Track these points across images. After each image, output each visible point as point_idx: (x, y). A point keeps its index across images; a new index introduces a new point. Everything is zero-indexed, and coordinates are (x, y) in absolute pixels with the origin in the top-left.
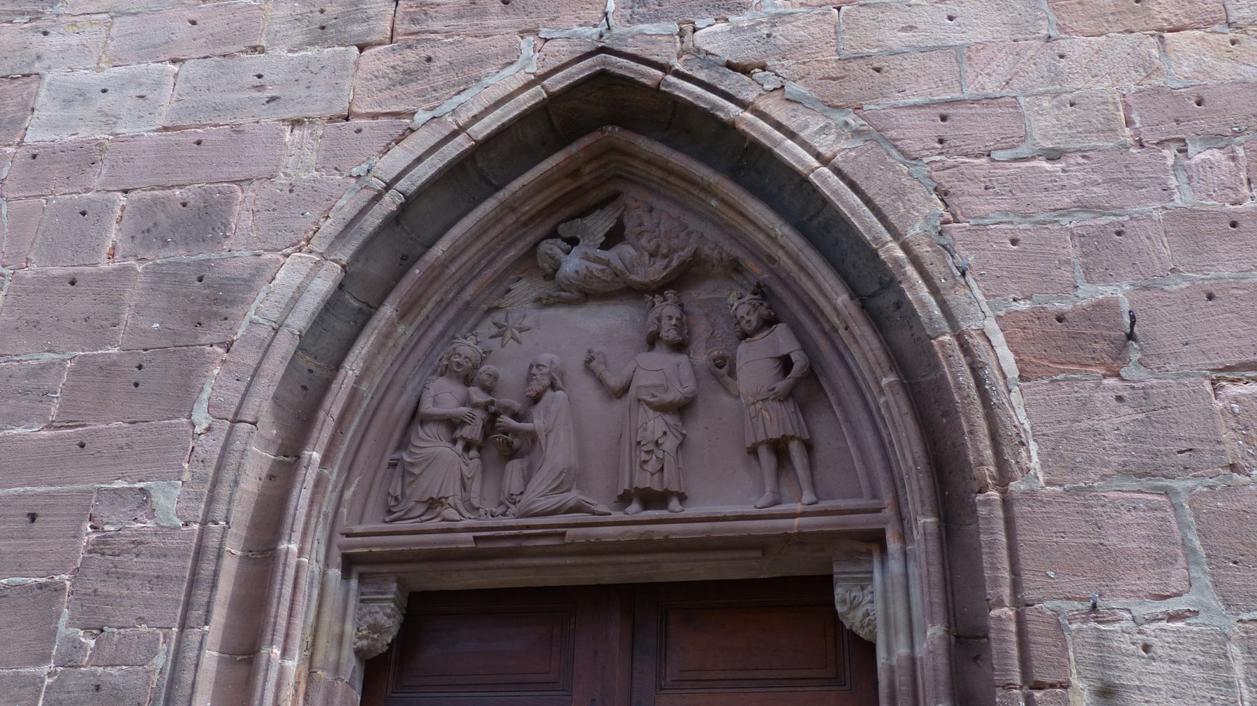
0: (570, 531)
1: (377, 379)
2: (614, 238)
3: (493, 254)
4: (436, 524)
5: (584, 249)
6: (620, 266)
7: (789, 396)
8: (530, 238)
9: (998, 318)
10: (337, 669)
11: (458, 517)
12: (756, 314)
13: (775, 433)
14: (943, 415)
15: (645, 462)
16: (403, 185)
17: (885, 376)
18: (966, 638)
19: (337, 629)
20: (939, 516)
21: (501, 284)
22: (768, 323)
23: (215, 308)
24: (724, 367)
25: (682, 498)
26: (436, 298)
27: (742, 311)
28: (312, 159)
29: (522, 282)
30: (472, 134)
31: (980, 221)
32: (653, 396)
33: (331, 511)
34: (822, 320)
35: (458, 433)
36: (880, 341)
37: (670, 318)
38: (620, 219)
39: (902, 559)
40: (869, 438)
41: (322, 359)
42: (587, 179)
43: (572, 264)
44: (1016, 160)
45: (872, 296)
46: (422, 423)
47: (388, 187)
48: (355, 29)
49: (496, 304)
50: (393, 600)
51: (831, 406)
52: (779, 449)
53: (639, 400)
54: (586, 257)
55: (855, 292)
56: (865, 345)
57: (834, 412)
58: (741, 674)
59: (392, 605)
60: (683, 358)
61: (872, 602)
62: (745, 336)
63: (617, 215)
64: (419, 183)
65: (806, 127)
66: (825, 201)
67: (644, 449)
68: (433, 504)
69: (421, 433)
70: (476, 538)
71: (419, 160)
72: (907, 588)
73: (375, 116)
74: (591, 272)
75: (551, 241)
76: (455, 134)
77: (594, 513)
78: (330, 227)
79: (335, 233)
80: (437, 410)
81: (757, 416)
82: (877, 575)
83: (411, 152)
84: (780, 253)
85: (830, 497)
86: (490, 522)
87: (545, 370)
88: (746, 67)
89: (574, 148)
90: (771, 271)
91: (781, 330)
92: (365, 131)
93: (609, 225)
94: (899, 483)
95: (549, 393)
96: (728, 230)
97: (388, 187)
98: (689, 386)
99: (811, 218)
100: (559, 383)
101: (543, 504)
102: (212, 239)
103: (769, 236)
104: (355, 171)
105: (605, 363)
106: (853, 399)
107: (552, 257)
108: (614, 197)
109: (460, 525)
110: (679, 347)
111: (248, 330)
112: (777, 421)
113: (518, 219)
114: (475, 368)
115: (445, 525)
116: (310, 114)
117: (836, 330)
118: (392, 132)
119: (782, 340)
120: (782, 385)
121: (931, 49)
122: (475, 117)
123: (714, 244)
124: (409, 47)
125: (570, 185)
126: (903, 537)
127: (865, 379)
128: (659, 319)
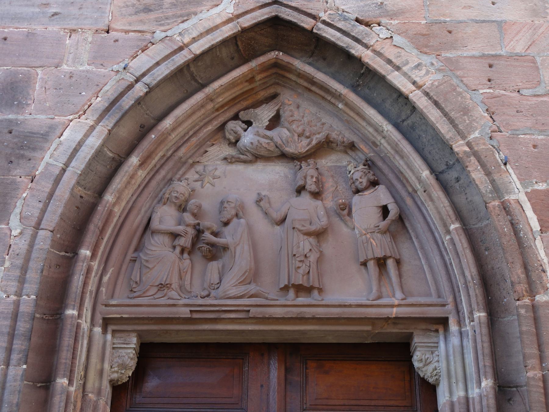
0: (253, 310)
1: (123, 204)
2: (275, 122)
3: (197, 127)
4: (163, 301)
5: (256, 130)
6: (279, 142)
7: (386, 231)
8: (221, 119)
9: (526, 193)
10: (99, 393)
11: (179, 298)
12: (366, 178)
13: (379, 254)
14: (486, 250)
15: (299, 267)
16: (146, 79)
17: (453, 223)
18: (503, 387)
19: (99, 367)
20: (487, 313)
21: (201, 149)
22: (374, 184)
23: (22, 152)
24: (345, 210)
25: (320, 290)
26: (161, 154)
27: (357, 176)
28: (85, 57)
30: (192, 50)
31: (515, 132)
32: (303, 226)
33: (94, 289)
34: (407, 185)
35: (177, 242)
36: (449, 201)
37: (312, 177)
38: (278, 111)
39: (459, 336)
40: (437, 261)
41: (89, 190)
42: (258, 83)
43: (248, 138)
44: (535, 96)
45: (442, 172)
46: (153, 232)
47: (137, 80)
49: (198, 160)
50: (134, 349)
51: (411, 238)
52: (381, 263)
53: (294, 228)
54: (258, 134)
55: (432, 171)
56: (437, 204)
57: (413, 243)
58: (353, 402)
59: (134, 352)
60: (319, 203)
61: (438, 361)
62: (357, 191)
63: (276, 108)
64: (159, 79)
65: (407, 63)
67: (298, 259)
68: (162, 286)
69: (152, 242)
70: (191, 311)
71: (158, 64)
72: (463, 354)
73: (127, 32)
74: (261, 144)
75: (233, 122)
76: (181, 49)
77: (267, 299)
78: (100, 103)
79: (103, 108)
80: (163, 227)
81: (367, 242)
82: (442, 345)
83: (152, 58)
85: (412, 295)
86: (201, 302)
87: (233, 205)
88: (368, 22)
89: (253, 64)
90: (375, 152)
91: (381, 190)
92: (120, 42)
93: (272, 114)
94: (456, 289)
95: (235, 220)
96: (348, 123)
97: (137, 80)
98: (324, 221)
99: (403, 121)
100: (241, 214)
101: (233, 292)
102: (18, 105)
103: (376, 130)
104: (116, 67)
105: (269, 203)
106: (426, 236)
107: (235, 133)
108: (274, 96)
109: (181, 302)
110: (316, 195)
111: (46, 168)
112: (379, 246)
113: (214, 106)
114: (187, 201)
115: (171, 302)
116: (83, 27)
117: (416, 192)
118: (139, 43)
119: (382, 195)
120: (383, 224)
121: (484, 21)
122: (194, 38)
123: (339, 131)
125: (247, 87)
126: (460, 323)
127: (434, 224)
128: (305, 178)
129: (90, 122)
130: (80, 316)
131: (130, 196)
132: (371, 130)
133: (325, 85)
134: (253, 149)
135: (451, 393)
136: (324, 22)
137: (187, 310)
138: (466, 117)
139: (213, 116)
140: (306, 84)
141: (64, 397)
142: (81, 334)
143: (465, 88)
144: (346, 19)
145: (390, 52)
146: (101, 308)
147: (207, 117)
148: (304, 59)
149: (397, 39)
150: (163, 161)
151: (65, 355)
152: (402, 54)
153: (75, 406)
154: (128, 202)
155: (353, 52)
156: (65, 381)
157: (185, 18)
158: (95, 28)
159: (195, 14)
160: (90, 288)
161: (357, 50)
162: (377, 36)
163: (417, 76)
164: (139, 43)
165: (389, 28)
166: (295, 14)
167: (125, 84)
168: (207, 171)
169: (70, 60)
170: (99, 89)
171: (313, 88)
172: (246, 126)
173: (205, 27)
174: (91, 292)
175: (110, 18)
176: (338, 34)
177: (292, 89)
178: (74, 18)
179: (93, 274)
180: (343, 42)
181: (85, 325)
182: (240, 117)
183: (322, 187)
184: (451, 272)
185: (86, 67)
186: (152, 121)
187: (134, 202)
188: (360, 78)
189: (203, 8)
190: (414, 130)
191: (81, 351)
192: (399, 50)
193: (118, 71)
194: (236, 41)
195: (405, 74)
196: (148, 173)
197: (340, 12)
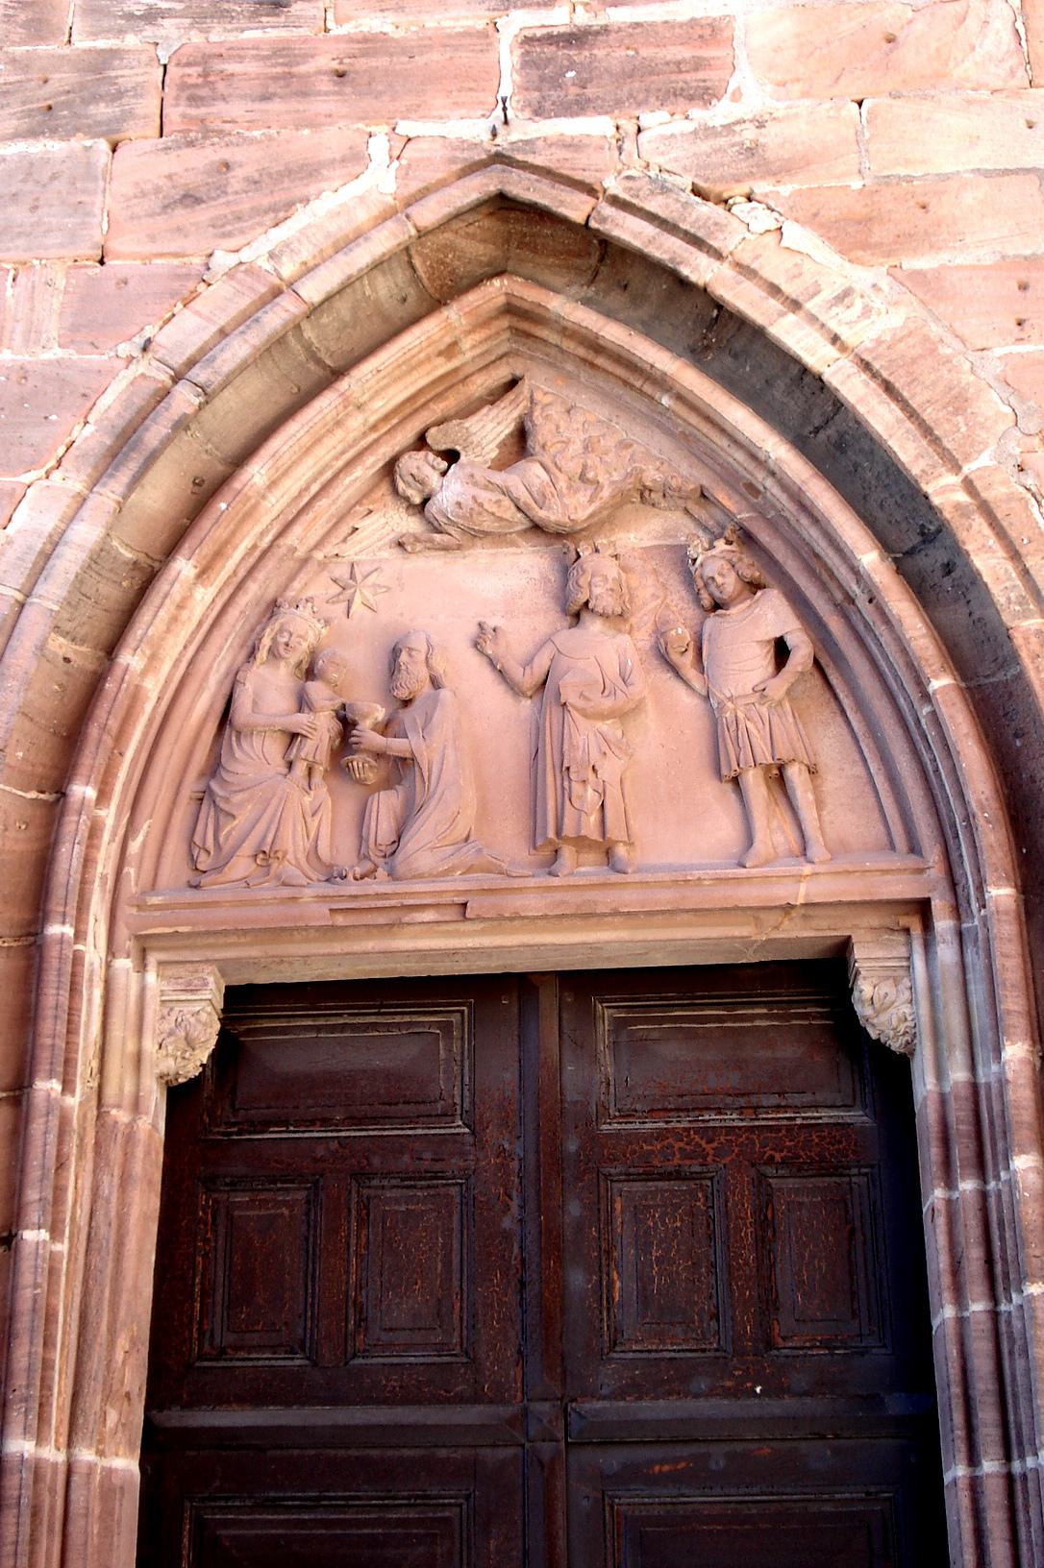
1: (166, 667)
3: (329, 474)
8: (385, 452)
14: (1016, 736)
17: (936, 677)
19: (131, 1047)
22: (754, 586)
26: (245, 545)
28: (52, 328)
29: (373, 517)
34: (832, 586)
39: (956, 946)
41: (83, 642)
42: (469, 355)
43: (451, 492)
48: (102, 111)
62: (717, 606)
63: (515, 414)
66: (838, 405)
69: (238, 754)
72: (965, 983)
74: (481, 505)
76: (276, 293)
78: (91, 436)
83: (209, 320)
84: (769, 483)
90: (753, 508)
99: (817, 430)
103: (753, 457)
104: (124, 349)
116: (42, 253)
117: (853, 602)
118: (176, 285)
121: (1007, 172)
124: (191, 144)
125: (443, 367)
127: (896, 676)
129: (77, 485)
130: (79, 935)
131: (180, 648)
132: (740, 456)
133: (624, 354)
134: (463, 517)
135: (940, 1074)
136: (615, 201)
137: (325, 909)
138: (960, 418)
139: (364, 443)
140: (582, 352)
141: (54, 1123)
142: (86, 975)
143: (959, 346)
144: (665, 190)
145: (773, 268)
146: (126, 911)
147: (351, 447)
148: (574, 289)
149: (792, 230)
150: (252, 560)
151: (50, 1027)
152: (805, 268)
153: (81, 1139)
154: (176, 665)
155: (685, 271)
156: (56, 1086)
157: (281, 215)
158: (70, 253)
159: (306, 201)
160: (100, 869)
161: (699, 269)
162: (743, 229)
163: (838, 320)
164: (176, 285)
165: (772, 205)
166: (545, 185)
167: (147, 389)
168: (359, 577)
169: (18, 338)
170: (89, 405)
171: (600, 361)
172: (444, 465)
173: (328, 235)
174: (104, 878)
175: (105, 227)
176: (649, 230)
177: (551, 365)
178: (19, 235)
179: (106, 836)
180: (665, 248)
181: (93, 953)
182: (429, 441)
183: (631, 601)
184: (937, 791)
185: (56, 353)
186: (221, 468)
187: (191, 663)
188: (710, 328)
189: (323, 185)
190: (843, 452)
191: (89, 1015)
192: (798, 259)
193: (131, 359)
194: (410, 257)
195: (813, 319)
196: (220, 591)
197: (652, 174)
